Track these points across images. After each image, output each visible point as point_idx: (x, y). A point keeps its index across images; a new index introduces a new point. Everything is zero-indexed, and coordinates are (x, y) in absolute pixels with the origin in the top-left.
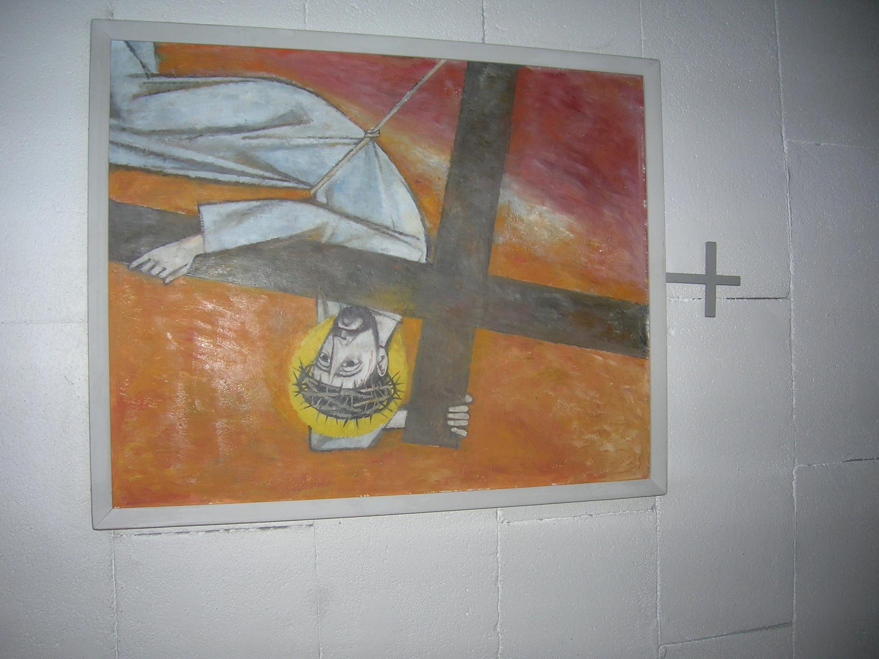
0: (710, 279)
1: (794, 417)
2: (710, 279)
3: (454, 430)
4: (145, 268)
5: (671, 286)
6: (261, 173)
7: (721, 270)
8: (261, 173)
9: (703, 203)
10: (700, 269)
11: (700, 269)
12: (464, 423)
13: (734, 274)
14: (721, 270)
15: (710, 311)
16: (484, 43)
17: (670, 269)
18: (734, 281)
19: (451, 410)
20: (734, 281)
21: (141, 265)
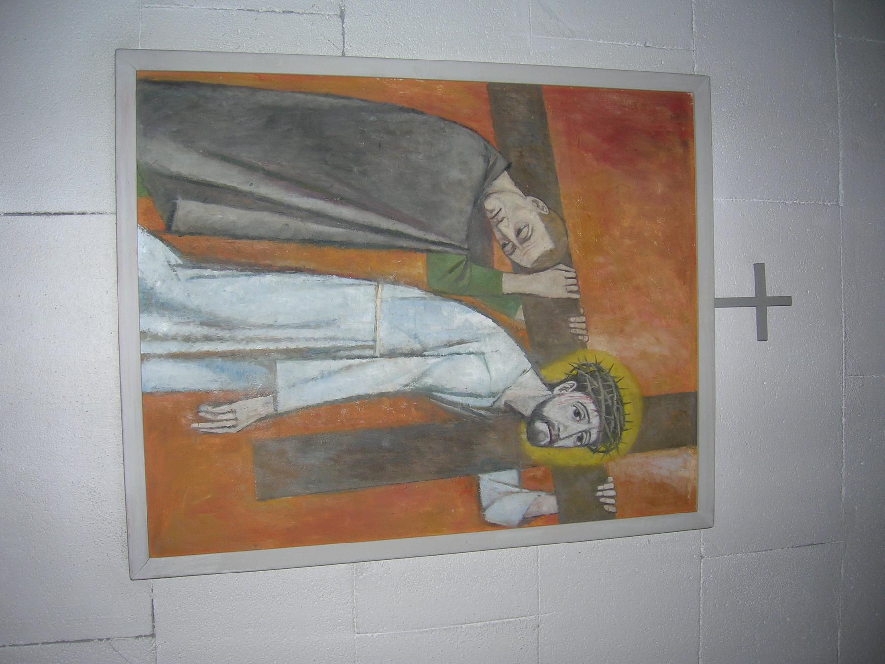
0: (761, 302)
1: (844, 419)
2: (761, 302)
3: (602, 500)
4: (575, 288)
5: (719, 311)
6: (443, 396)
7: (771, 291)
8: (443, 396)
9: (742, 209)
10: (749, 291)
11: (749, 291)
12: (613, 493)
13: (785, 293)
14: (771, 291)
15: (762, 336)
16: (343, 55)
17: (719, 294)
18: (786, 301)
19: (600, 488)
20: (786, 301)
21: (576, 292)
